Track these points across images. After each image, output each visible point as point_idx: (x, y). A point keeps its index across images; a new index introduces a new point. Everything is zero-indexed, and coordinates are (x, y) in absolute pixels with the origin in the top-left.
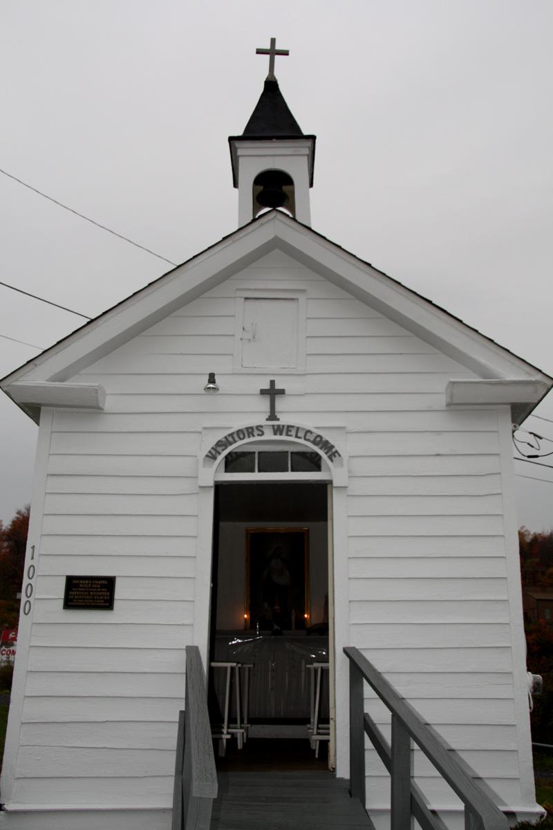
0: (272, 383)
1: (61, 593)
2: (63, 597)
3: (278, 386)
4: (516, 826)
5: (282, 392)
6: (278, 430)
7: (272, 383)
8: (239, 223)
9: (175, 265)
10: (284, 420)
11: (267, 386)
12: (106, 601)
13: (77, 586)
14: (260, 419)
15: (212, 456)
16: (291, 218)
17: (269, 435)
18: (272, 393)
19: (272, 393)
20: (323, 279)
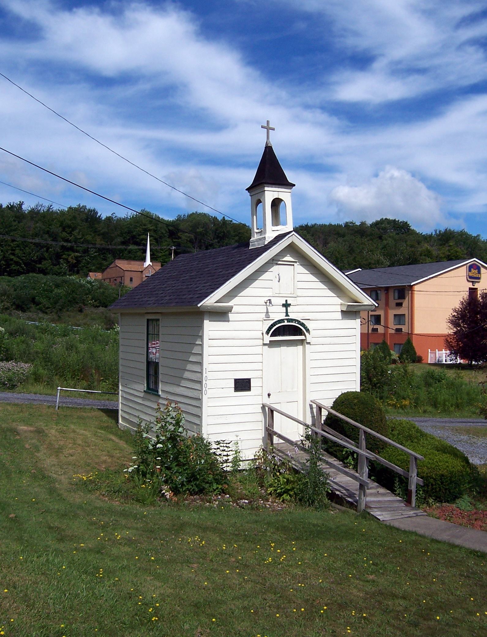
0: (286, 301)
1: (233, 385)
2: (234, 386)
3: (288, 303)
4: (335, 225)
5: (290, 305)
6: (289, 320)
7: (286, 301)
8: (294, 223)
9: (246, 165)
10: (292, 316)
11: (285, 303)
12: (248, 387)
13: (238, 382)
14: (283, 316)
15: (267, 333)
16: (426, 515)
17: (286, 323)
18: (286, 305)
19: (286, 305)
20: (308, 272)
